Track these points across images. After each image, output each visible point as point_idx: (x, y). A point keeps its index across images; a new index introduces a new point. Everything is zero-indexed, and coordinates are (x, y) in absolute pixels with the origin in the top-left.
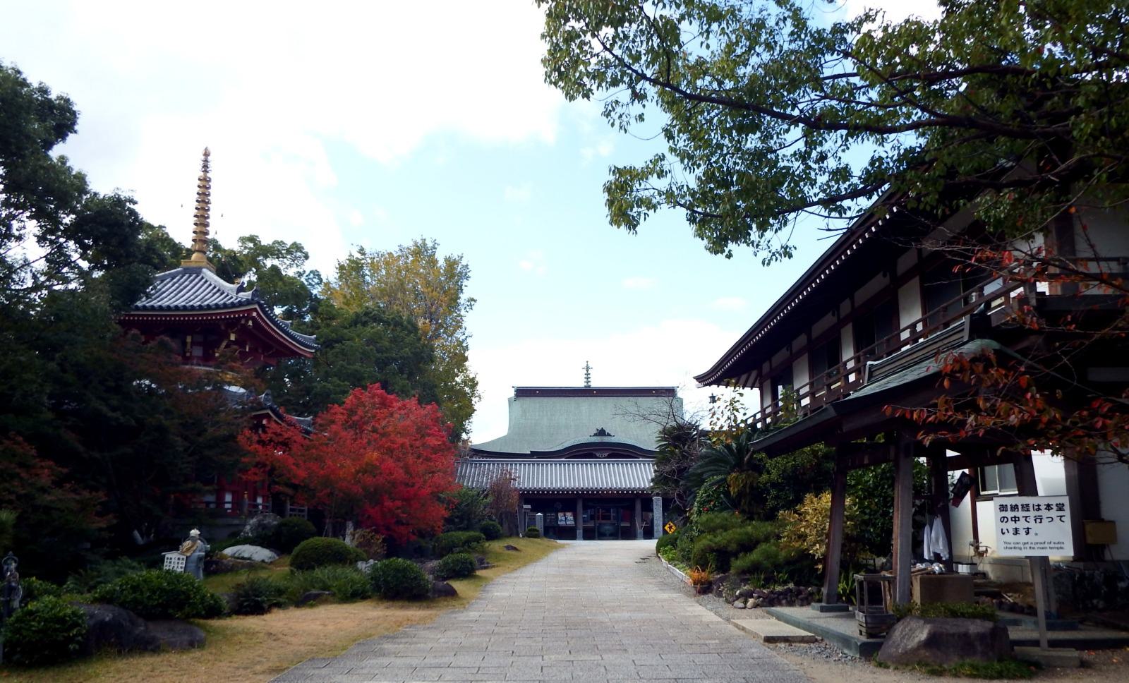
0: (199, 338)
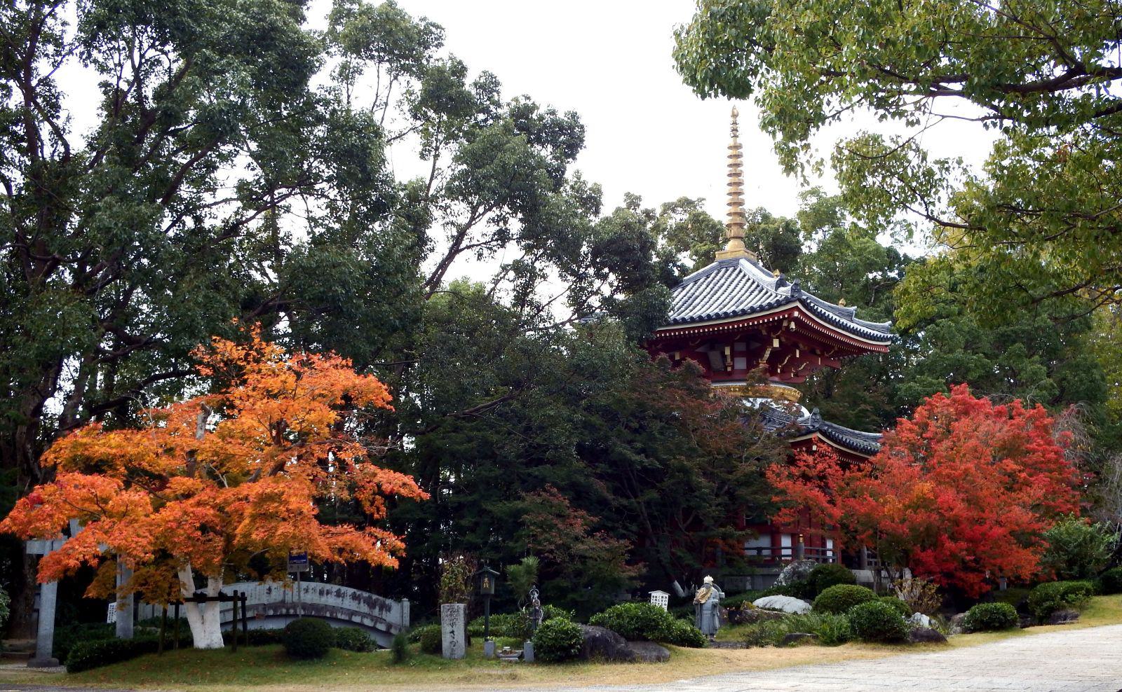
0: (741, 347)
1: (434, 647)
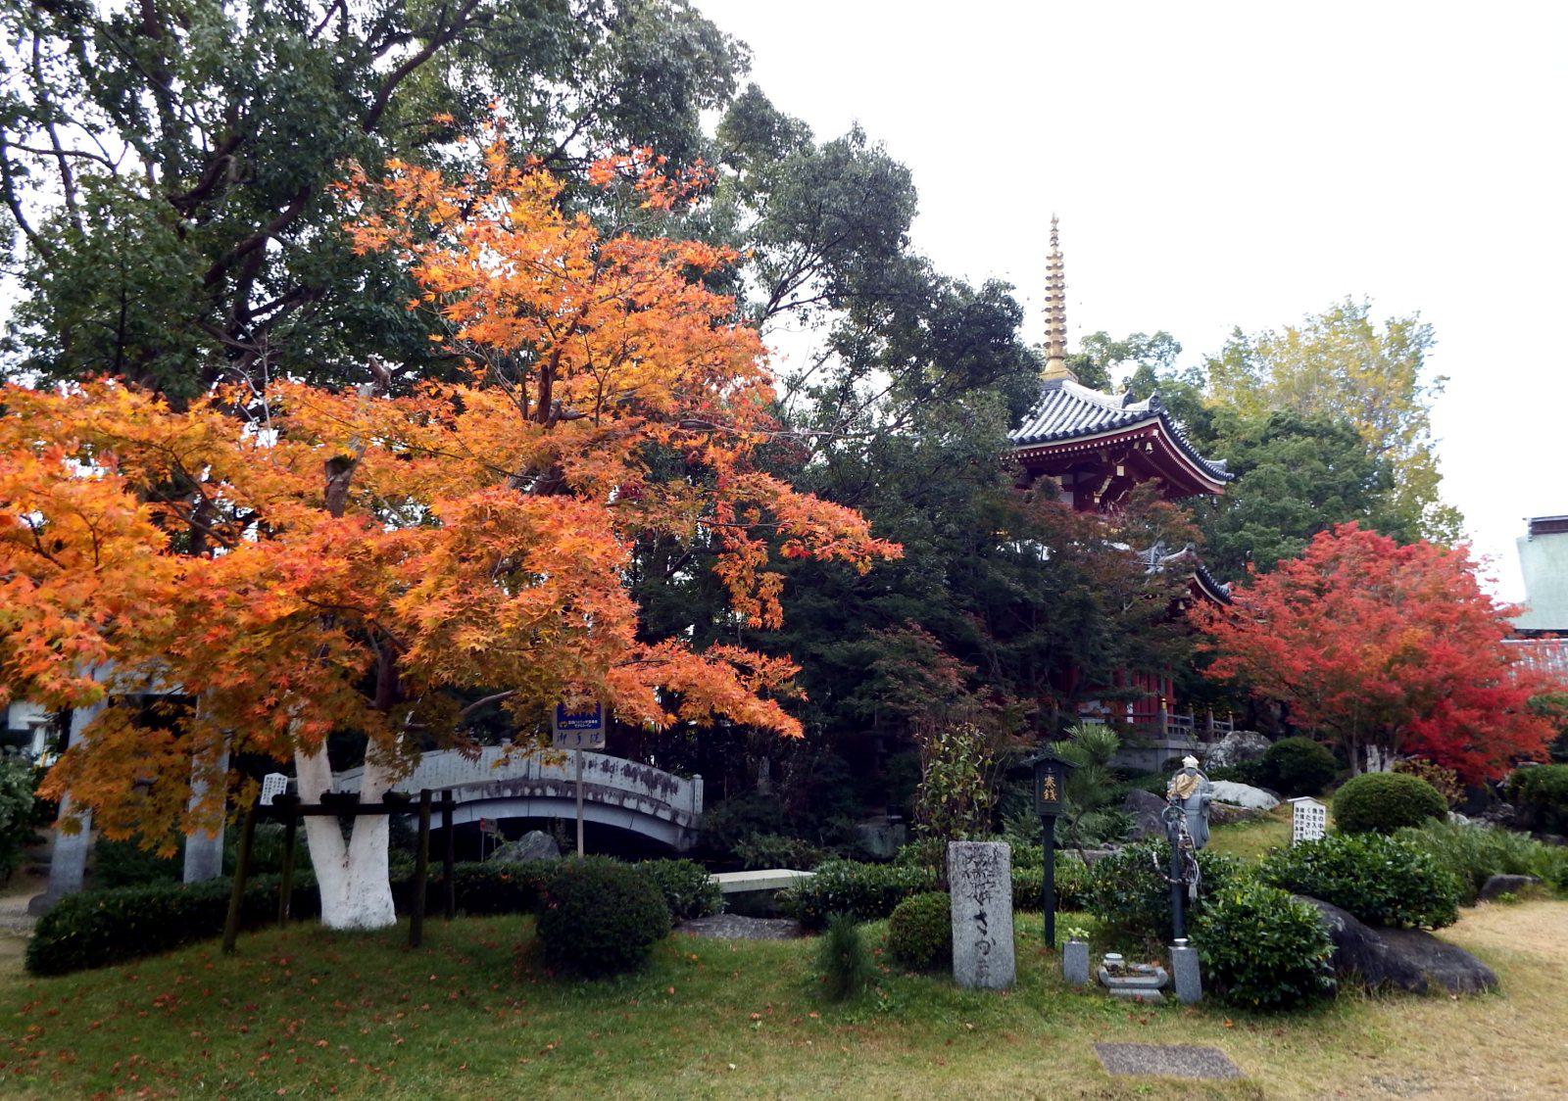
1: (928, 952)
